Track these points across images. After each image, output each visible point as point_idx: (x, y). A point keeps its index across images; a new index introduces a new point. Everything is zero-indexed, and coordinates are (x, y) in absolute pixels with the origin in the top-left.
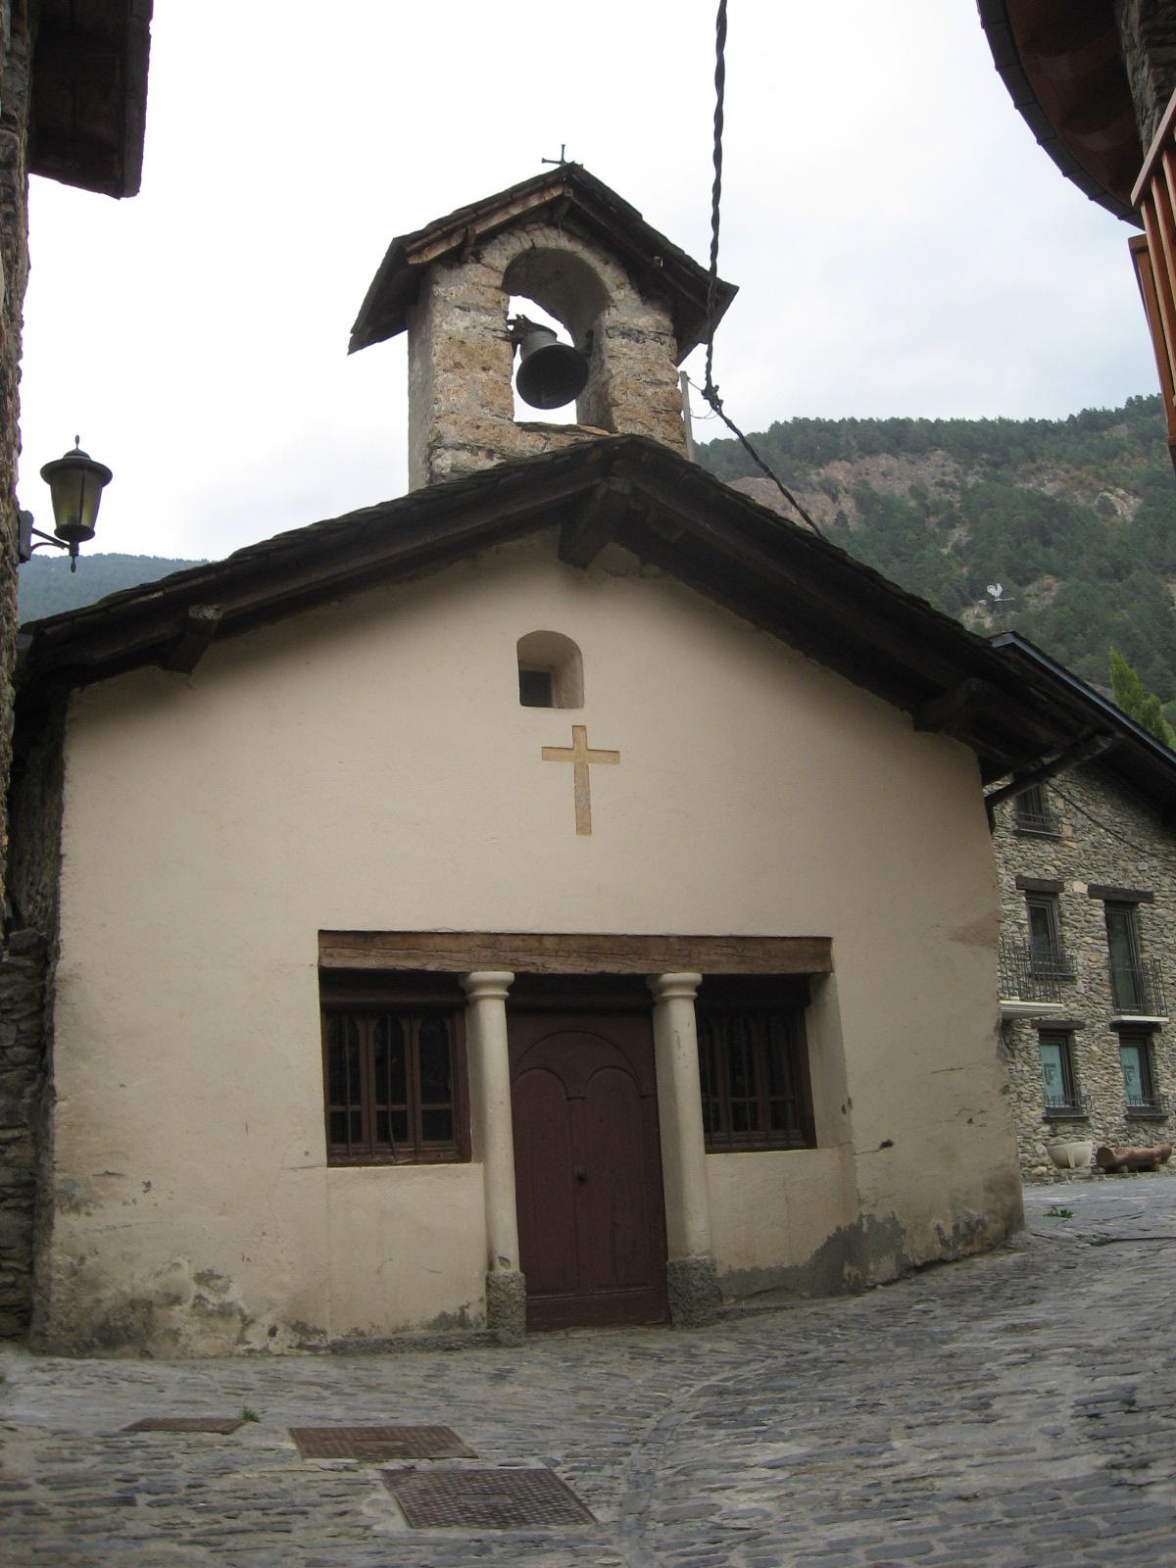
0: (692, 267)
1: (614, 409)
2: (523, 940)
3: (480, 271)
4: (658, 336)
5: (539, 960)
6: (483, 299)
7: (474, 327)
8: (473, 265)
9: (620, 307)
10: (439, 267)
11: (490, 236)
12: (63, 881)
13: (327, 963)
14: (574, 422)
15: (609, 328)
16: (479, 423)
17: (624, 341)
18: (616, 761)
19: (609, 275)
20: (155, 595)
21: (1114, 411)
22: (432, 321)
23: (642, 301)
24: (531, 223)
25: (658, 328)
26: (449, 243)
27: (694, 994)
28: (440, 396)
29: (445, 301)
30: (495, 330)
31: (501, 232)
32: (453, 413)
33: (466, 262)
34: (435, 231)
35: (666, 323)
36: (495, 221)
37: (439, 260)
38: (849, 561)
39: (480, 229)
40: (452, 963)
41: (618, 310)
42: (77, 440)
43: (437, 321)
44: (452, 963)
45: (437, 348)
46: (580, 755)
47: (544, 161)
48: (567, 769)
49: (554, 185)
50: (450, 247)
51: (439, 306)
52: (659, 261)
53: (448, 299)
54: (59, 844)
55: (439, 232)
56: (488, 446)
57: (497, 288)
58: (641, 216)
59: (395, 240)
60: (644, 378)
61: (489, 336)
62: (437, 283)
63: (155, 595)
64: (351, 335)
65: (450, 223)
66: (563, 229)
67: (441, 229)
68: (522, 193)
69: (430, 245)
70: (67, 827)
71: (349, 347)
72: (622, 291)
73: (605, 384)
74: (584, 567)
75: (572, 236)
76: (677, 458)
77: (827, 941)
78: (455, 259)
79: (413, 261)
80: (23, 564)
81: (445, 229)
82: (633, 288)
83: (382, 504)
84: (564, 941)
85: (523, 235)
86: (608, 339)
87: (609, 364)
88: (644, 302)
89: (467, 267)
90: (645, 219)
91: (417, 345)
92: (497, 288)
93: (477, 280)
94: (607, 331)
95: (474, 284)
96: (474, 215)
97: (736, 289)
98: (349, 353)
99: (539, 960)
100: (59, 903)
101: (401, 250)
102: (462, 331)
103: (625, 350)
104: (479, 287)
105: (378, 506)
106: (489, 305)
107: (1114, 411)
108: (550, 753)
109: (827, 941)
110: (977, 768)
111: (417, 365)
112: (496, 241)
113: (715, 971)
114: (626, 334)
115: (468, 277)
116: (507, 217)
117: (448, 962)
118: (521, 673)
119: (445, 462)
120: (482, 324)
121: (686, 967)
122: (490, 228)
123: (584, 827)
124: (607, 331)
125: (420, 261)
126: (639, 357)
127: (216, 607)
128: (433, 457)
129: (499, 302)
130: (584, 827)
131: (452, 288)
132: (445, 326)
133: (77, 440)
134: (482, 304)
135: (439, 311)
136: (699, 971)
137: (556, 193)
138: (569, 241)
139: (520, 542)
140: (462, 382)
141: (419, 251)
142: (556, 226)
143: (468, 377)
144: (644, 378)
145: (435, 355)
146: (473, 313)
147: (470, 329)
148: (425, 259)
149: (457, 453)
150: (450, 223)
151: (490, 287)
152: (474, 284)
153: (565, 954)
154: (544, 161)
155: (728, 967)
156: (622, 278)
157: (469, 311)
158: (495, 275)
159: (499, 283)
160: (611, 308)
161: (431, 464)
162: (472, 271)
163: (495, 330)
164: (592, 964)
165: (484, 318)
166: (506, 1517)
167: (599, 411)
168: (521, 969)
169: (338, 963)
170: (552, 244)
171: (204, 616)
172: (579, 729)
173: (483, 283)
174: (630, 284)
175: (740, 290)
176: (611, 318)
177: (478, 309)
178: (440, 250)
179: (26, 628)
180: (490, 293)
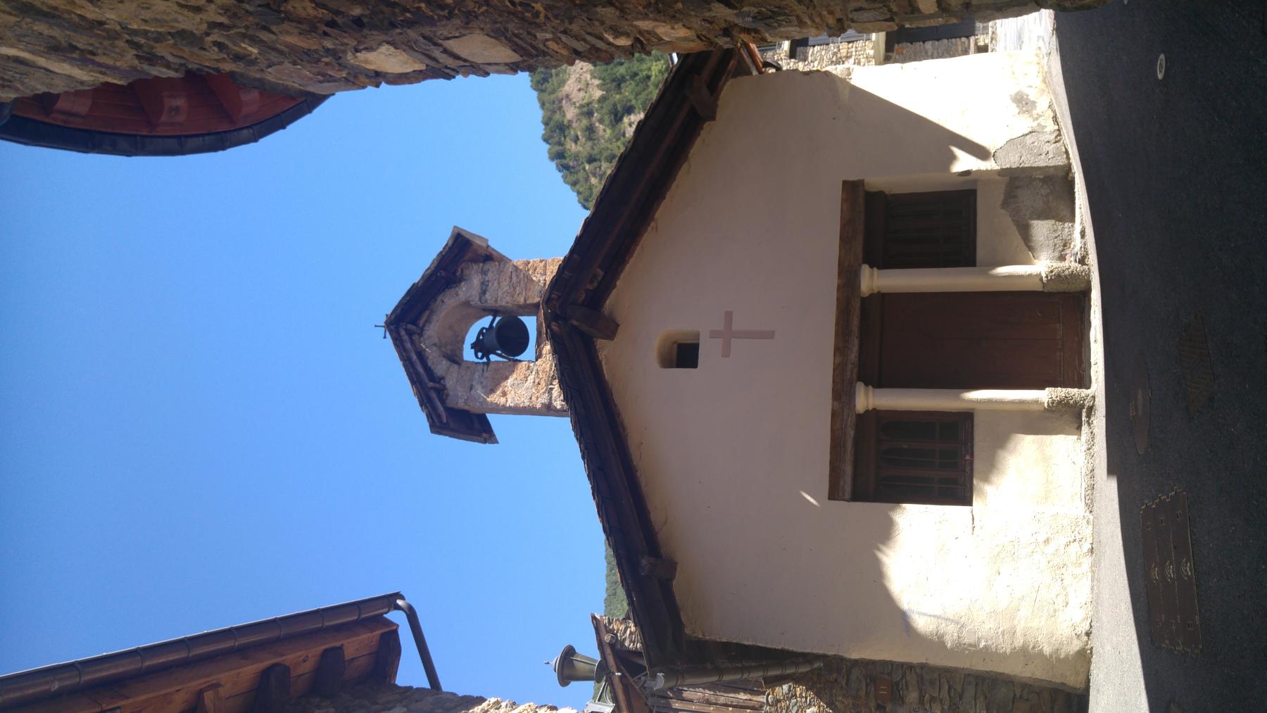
4: (484, 273)
7: (482, 383)
10: (448, 401)
13: (848, 496)
14: (535, 318)
17: (488, 293)
21: (519, 72)
30: (483, 371)
31: (427, 364)
32: (531, 398)
33: (444, 386)
36: (420, 369)
37: (443, 402)
38: (614, 172)
40: (850, 419)
44: (850, 419)
46: (727, 334)
47: (385, 337)
48: (736, 343)
49: (398, 333)
59: (432, 432)
65: (422, 397)
67: (426, 401)
69: (434, 408)
71: (493, 443)
72: (459, 293)
77: (845, 183)
78: (441, 392)
83: (583, 457)
84: (840, 349)
89: (448, 386)
93: (454, 379)
98: (498, 443)
99: (850, 366)
101: (438, 426)
106: (469, 373)
107: (519, 72)
108: (726, 353)
109: (845, 183)
110: (740, 78)
113: (861, 256)
114: (484, 292)
116: (417, 361)
117: (849, 422)
118: (678, 366)
119: (558, 404)
123: (770, 335)
129: (467, 367)
130: (770, 335)
136: (860, 266)
137: (403, 333)
139: (603, 363)
141: (439, 416)
142: (422, 329)
149: (553, 398)
154: (385, 337)
156: (453, 291)
158: (451, 369)
162: (450, 383)
163: (483, 371)
165: (476, 376)
166: (776, 705)
167: (532, 309)
168: (855, 377)
172: (714, 335)
175: (456, 225)
177: (471, 380)
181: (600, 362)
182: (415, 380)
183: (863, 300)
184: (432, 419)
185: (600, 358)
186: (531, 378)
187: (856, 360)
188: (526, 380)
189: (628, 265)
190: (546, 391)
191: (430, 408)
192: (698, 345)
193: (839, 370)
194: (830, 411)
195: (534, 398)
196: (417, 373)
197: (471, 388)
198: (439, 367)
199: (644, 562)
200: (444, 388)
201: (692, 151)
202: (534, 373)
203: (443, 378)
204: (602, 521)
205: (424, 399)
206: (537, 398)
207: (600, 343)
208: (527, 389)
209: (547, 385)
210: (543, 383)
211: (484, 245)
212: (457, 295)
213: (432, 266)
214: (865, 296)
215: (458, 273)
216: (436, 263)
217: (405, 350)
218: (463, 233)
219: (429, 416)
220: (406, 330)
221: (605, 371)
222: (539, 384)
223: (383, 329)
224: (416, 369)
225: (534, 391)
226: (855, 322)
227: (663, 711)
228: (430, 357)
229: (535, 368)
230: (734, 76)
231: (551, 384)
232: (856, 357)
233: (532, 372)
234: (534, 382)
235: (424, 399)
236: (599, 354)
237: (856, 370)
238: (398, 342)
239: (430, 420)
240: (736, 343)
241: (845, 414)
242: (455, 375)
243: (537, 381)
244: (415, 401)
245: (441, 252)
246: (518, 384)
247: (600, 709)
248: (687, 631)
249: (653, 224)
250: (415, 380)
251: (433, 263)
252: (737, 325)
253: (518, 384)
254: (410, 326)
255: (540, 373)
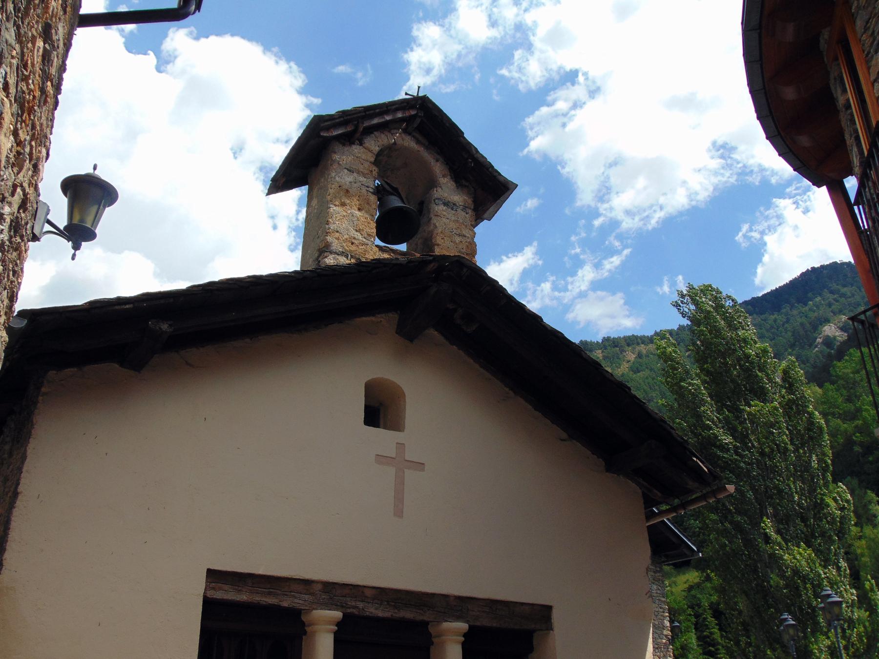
0: (490, 169)
1: (436, 247)
2: (351, 589)
3: (362, 150)
4: (465, 208)
5: (361, 605)
6: (362, 166)
7: (355, 183)
8: (358, 146)
9: (443, 188)
11: (369, 131)
12: (16, 512)
13: (211, 594)
15: (436, 199)
16: (353, 241)
17: (445, 208)
18: (423, 470)
19: (438, 168)
20: (127, 306)
22: (329, 174)
23: (457, 186)
24: (395, 129)
25: (465, 204)
26: (346, 128)
27: (463, 639)
28: (330, 220)
29: (339, 164)
30: (368, 187)
31: (377, 131)
32: (337, 232)
33: (354, 144)
34: (340, 117)
35: (470, 201)
37: (338, 138)
39: (367, 124)
40: (301, 602)
41: (442, 189)
42: (95, 168)
43: (333, 174)
44: (301, 602)
45: (331, 191)
48: (391, 471)
50: (346, 131)
51: (335, 166)
52: (471, 163)
53: (341, 163)
54: (18, 484)
55: (342, 119)
56: (357, 256)
57: (370, 162)
58: (463, 133)
60: (455, 231)
61: (364, 190)
62: (335, 153)
63: (127, 306)
64: (271, 182)
65: (350, 115)
66: (414, 136)
68: (394, 107)
69: (336, 126)
70: (27, 471)
72: (446, 179)
73: (431, 233)
74: (411, 341)
75: (418, 142)
76: (484, 275)
77: (549, 608)
78: (348, 139)
79: (324, 134)
80: (41, 196)
81: (345, 118)
82: (452, 178)
84: (383, 594)
85: (389, 135)
86: (435, 205)
87: (435, 220)
88: (458, 187)
89: (354, 147)
90: (465, 136)
91: (315, 191)
92: (370, 162)
94: (434, 200)
95: (357, 157)
96: (364, 114)
97: (516, 186)
98: (268, 194)
99: (361, 605)
100: (9, 529)
102: (348, 183)
103: (445, 213)
104: (361, 160)
105: (292, 272)
106: (366, 172)
108: (381, 459)
109: (549, 608)
111: (315, 202)
112: (373, 135)
113: (478, 624)
114: (446, 204)
115: (354, 152)
117: (298, 601)
120: (360, 182)
121: (458, 618)
122: (372, 125)
123: (399, 512)
124: (434, 200)
125: (328, 135)
126: (453, 218)
127: (169, 323)
128: (321, 257)
129: (372, 171)
130: (399, 512)
131: (344, 157)
132: (337, 179)
133: (95, 168)
134: (362, 170)
135: (334, 169)
136: (467, 622)
138: (416, 144)
139: (373, 318)
140: (345, 214)
141: (328, 129)
142: (410, 134)
143: (349, 212)
144: (455, 231)
145: (329, 195)
146: (355, 174)
147: (353, 183)
148: (331, 134)
149: (337, 257)
150: (350, 115)
151: (367, 161)
152: (357, 157)
153: (379, 602)
154: (406, 94)
155: (485, 621)
156: (447, 172)
157: (353, 172)
158: (370, 154)
159: (373, 160)
160: (438, 188)
161: (319, 262)
162: (356, 149)
163: (368, 187)
164: (396, 611)
165: (362, 179)
168: (349, 611)
169: (219, 595)
170: (406, 144)
171: (160, 328)
172: (401, 446)
173: (363, 158)
174: (451, 176)
176: (437, 193)
177: (358, 172)
178: (340, 131)
179: (23, 314)
180: (367, 164)
181: (373, 315)
182: (367, 113)
183: (425, 624)
184: (327, 121)
185: (379, 316)
186: (358, 236)
187: (368, 613)
188: (357, 231)
189: (472, 361)
190: (345, 250)
191: (337, 121)
192: (378, 427)
193: (355, 590)
194: (449, 594)
195: (337, 235)
196: (372, 117)
197: (351, 171)
198: (373, 142)
199: (165, 327)
200: (352, 143)
201: (579, 445)
202: (364, 240)
203: (361, 144)
204: (267, 276)
205: (349, 117)
206: (338, 239)
207: (394, 317)
208: (348, 230)
209: (351, 251)
210: (353, 248)
211: (486, 215)
212: (444, 176)
213: (479, 156)
214: (466, 631)
215: (464, 182)
216: (481, 160)
217: (397, 110)
218: (509, 192)
219: (330, 118)
220: (415, 116)
221: (364, 319)
222: (352, 243)
223: (415, 94)
224: (376, 117)
225: (346, 236)
226: (407, 614)
227: (847, 137)
228: (383, 136)
229: (369, 243)
230: (644, 494)
231: (352, 257)
232: (372, 613)
233: (364, 238)
234: (354, 238)
235: (349, 117)
236: (383, 315)
237: (355, 611)
238: (405, 104)
239: (327, 118)
240: (391, 471)
241: (307, 597)
242: (364, 157)
243: (356, 242)
244: (348, 106)
245: (492, 167)
246: (353, 221)
247: (40, 219)
248: (52, 374)
249: (511, 393)
250: (367, 113)
251: (483, 157)
252: (410, 475)
253: (353, 221)
254: (418, 121)
255: (364, 247)
